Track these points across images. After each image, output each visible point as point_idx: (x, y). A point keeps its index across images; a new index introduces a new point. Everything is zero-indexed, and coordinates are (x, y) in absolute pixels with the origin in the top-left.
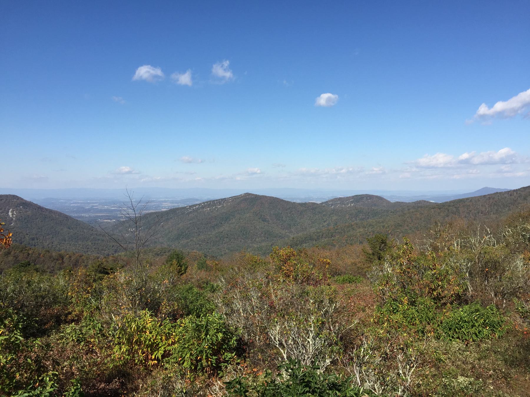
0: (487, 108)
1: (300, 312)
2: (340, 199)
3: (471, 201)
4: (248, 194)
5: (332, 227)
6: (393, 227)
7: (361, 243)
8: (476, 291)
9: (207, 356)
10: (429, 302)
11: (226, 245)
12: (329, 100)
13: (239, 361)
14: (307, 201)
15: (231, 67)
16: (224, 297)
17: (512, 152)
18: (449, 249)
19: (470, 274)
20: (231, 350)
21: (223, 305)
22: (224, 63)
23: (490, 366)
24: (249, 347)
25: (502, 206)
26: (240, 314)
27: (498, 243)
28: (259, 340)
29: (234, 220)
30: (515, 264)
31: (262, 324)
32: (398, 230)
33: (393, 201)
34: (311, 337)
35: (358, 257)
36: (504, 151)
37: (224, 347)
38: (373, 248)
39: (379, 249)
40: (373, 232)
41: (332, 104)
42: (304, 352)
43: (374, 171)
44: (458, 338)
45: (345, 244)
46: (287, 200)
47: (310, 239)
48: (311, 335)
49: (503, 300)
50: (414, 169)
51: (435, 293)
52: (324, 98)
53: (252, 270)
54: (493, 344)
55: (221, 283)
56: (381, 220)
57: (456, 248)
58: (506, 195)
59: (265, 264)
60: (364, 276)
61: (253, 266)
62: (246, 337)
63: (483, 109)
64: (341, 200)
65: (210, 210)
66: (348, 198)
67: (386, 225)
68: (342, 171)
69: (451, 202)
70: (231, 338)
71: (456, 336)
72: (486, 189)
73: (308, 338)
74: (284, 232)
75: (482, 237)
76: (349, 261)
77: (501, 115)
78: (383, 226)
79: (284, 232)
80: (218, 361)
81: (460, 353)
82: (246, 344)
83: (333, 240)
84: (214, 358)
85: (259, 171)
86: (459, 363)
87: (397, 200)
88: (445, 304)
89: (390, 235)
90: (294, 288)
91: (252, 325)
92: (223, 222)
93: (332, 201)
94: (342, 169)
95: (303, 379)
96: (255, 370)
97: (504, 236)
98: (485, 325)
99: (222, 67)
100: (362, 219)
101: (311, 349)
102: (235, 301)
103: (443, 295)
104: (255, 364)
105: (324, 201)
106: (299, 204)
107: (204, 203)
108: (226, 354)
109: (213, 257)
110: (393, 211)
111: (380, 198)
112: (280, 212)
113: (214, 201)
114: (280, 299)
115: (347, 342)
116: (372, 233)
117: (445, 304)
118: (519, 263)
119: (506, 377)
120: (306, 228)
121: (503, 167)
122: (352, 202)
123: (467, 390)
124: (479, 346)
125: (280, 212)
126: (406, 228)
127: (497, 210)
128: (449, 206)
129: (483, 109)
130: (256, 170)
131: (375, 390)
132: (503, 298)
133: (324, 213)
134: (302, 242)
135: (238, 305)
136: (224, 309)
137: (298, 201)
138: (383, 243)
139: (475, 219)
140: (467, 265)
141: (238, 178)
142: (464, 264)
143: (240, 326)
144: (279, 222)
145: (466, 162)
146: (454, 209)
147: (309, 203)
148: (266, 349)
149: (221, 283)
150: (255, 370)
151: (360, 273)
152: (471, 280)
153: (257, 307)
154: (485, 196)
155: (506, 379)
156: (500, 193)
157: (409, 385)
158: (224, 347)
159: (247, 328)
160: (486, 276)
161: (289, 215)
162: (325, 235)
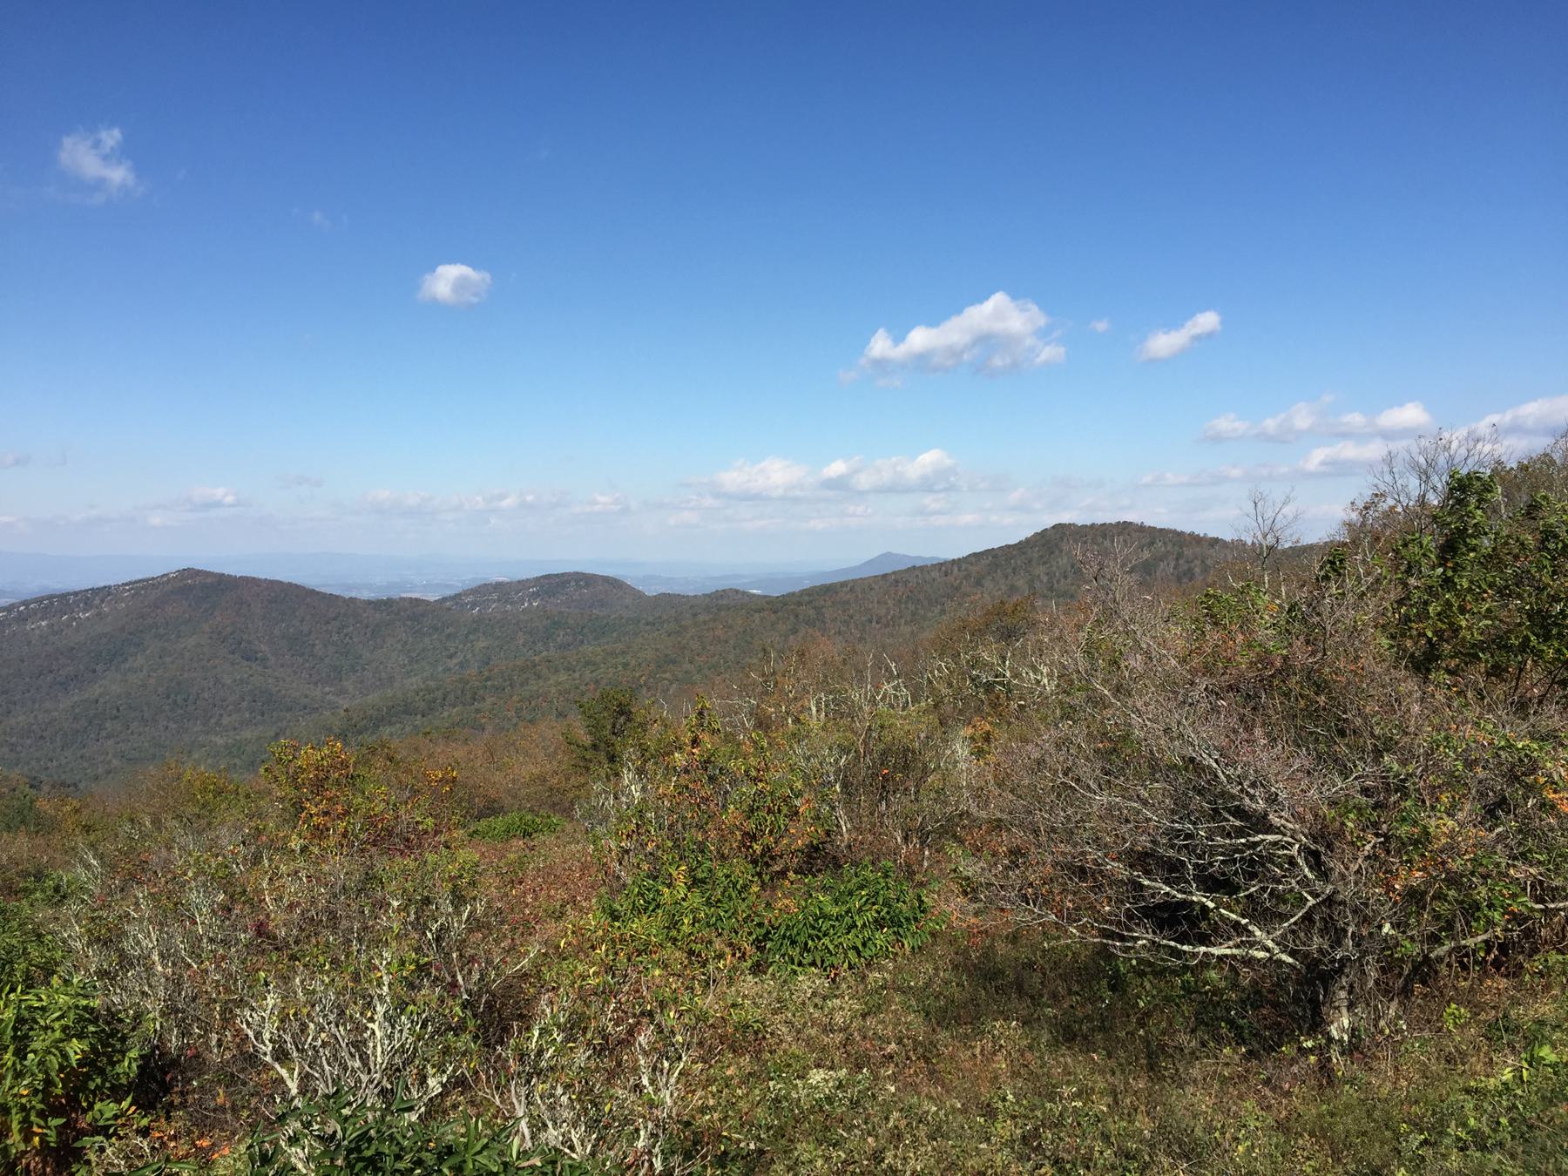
0: (889, 343)
1: (360, 940)
2: (498, 586)
3: (851, 590)
4: (189, 573)
5: (473, 670)
6: (653, 666)
7: (561, 715)
8: (858, 830)
9: (26, 1121)
10: (740, 869)
11: (110, 742)
12: (461, 285)
13: (145, 1122)
14: (395, 594)
15: (125, 152)
16: (93, 919)
17: (949, 462)
18: (797, 721)
19: (845, 786)
20: (117, 1093)
21: (89, 944)
22: (104, 135)
23: (889, 1032)
24: (182, 1073)
25: (925, 603)
26: (149, 969)
27: (916, 700)
28: (219, 1044)
29: (140, 660)
30: (948, 752)
31: (227, 991)
32: (667, 675)
33: (651, 591)
34: (379, 1017)
35: (551, 757)
36: (930, 458)
37: (92, 1086)
38: (594, 727)
39: (611, 731)
40: (597, 682)
41: (475, 300)
42: (358, 1064)
43: (595, 503)
44: (813, 964)
45: (515, 720)
46: (328, 591)
47: (405, 712)
48: (380, 1009)
49: (922, 850)
50: (709, 501)
51: (757, 848)
52: (447, 279)
53: (201, 821)
54: (899, 969)
55: (86, 871)
56: (620, 646)
57: (815, 718)
58: (935, 574)
59: (248, 796)
60: (567, 812)
61: (200, 810)
62: (173, 1042)
63: (880, 345)
64: (502, 590)
65: (50, 626)
66: (523, 584)
67: (633, 663)
68: (506, 503)
69: (803, 593)
70: (123, 1053)
71: (808, 959)
72: (887, 556)
73: (372, 1020)
74: (317, 693)
75: (877, 688)
76: (527, 770)
77: (922, 362)
78: (625, 665)
79: (317, 693)
80: (71, 1133)
81: (816, 1005)
82: (175, 1063)
83: (478, 711)
84: (55, 1122)
85: (230, 499)
86: (813, 1032)
87: (663, 590)
88: (783, 874)
89: (644, 690)
90: (340, 867)
91: (194, 1000)
92: (98, 668)
93: (475, 591)
94: (503, 497)
95: (358, 1149)
96: (205, 1143)
97: (930, 682)
98: (879, 924)
99: (97, 144)
100: (563, 647)
101: (379, 1058)
102: (131, 929)
103: (777, 851)
104: (204, 1123)
105: (449, 593)
106: (369, 602)
107: (26, 603)
108: (98, 1106)
109: (63, 784)
110: (651, 619)
111: (614, 584)
112: (306, 629)
113: (64, 597)
114: (291, 907)
115: (498, 1016)
116: (592, 686)
117: (783, 874)
118: (961, 750)
119: (927, 1053)
120: (391, 679)
121: (927, 500)
122: (535, 595)
123: (831, 1103)
124: (864, 978)
125: (306, 629)
126: (687, 666)
127: (914, 614)
128: (799, 604)
129: (880, 345)
130: (220, 492)
131: (572, 1148)
132: (922, 843)
133: (451, 630)
134: (380, 721)
135: (144, 939)
136: (95, 959)
137: (365, 595)
138: (622, 713)
139: (861, 639)
140: (836, 761)
141: (156, 520)
142: (832, 762)
143: (153, 1008)
144: (301, 660)
145: (839, 485)
146: (812, 612)
147: (402, 599)
148: (243, 1070)
149: (86, 871)
150: (205, 1143)
151: (559, 803)
152: (847, 803)
153: (211, 940)
154: (885, 576)
155: (927, 1061)
156: (922, 568)
157: (670, 1117)
158: (92, 1086)
159: (177, 1011)
160: (884, 789)
161: (335, 638)
162: (451, 697)
